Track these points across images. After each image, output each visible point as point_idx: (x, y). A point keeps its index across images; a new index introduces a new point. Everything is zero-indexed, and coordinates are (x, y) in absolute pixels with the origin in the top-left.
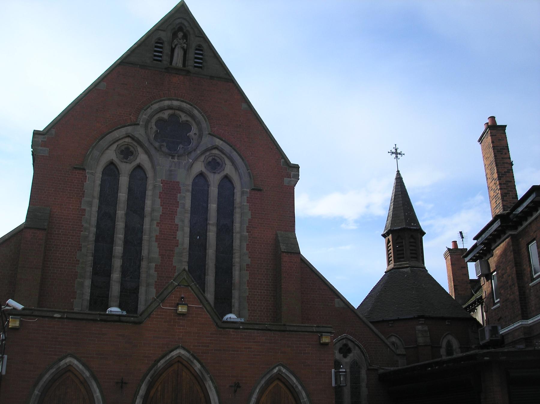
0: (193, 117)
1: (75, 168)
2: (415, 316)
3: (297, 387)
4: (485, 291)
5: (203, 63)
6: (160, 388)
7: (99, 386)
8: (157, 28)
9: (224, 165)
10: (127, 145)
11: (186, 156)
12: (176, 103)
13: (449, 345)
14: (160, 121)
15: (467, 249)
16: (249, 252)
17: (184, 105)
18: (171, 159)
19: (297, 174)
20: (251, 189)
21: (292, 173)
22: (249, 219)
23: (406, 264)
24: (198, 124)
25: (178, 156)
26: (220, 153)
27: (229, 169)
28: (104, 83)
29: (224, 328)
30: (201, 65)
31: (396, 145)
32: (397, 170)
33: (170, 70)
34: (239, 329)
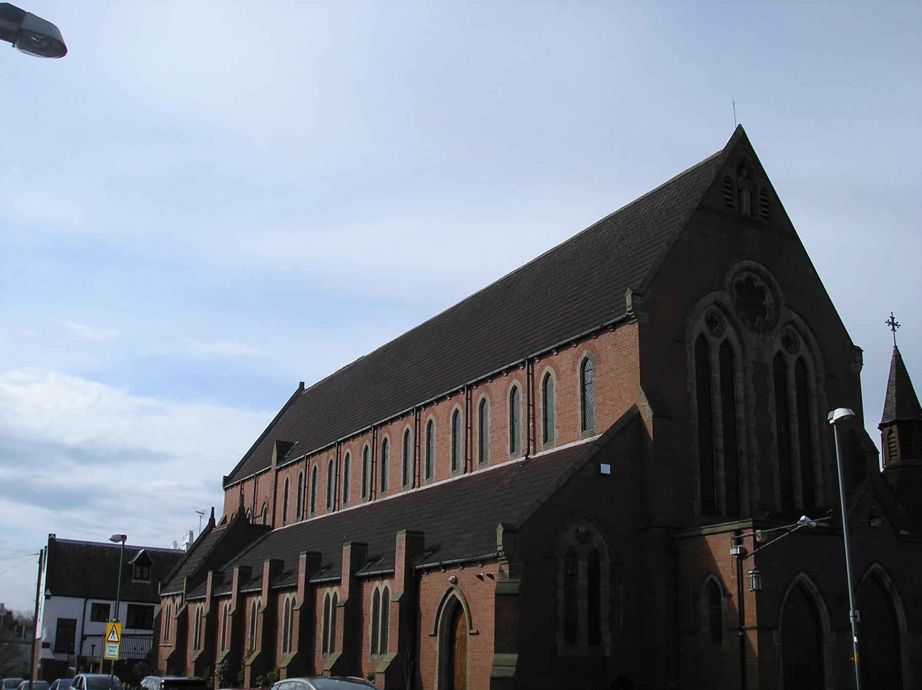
14: (739, 284)
15: (633, 417)
27: (803, 349)
31: (892, 313)
32: (894, 345)
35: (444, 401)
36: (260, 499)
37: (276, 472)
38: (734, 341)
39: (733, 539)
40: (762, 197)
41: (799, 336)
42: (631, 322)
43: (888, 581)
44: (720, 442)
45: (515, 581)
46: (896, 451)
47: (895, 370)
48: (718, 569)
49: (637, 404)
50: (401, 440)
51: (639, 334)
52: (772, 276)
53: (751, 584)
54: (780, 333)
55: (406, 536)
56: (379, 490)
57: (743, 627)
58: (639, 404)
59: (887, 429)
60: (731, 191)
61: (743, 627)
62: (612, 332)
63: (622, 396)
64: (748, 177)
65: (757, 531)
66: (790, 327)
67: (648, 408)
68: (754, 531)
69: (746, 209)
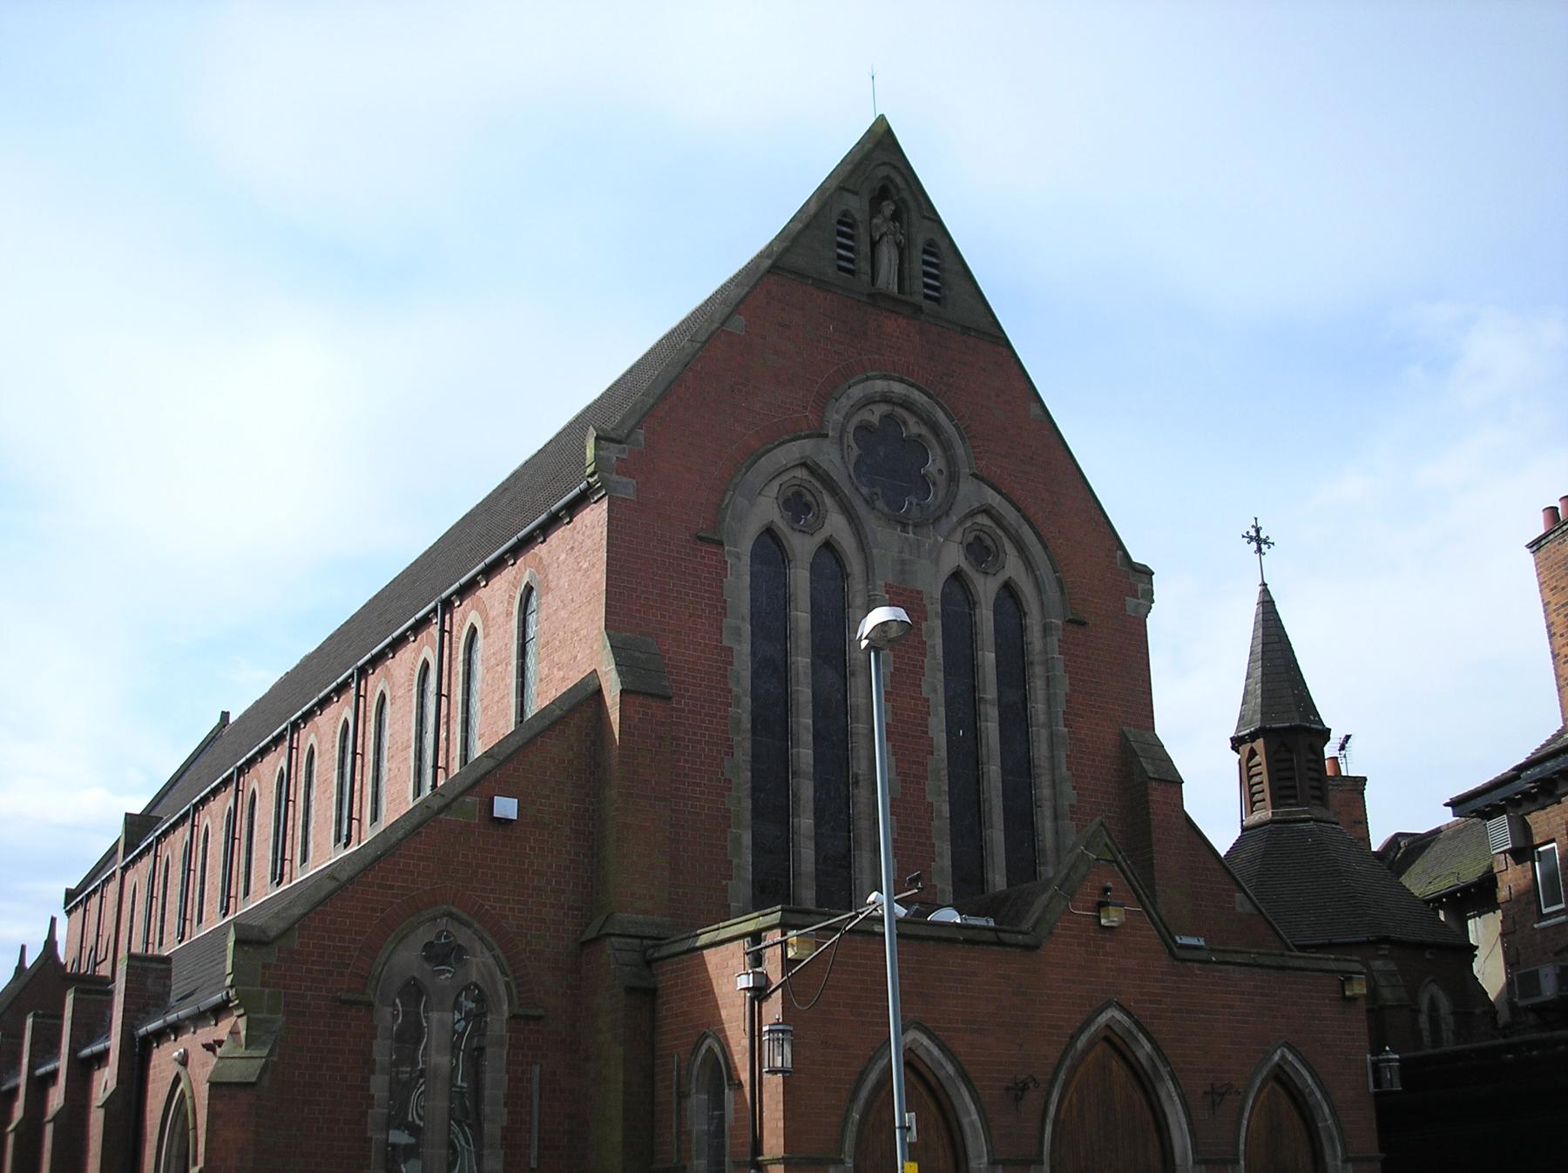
0: (935, 428)
1: (701, 539)
2: (1371, 938)
3: (1312, 1093)
4: (1509, 886)
5: (942, 291)
6: (1074, 1101)
7: (976, 1100)
8: (842, 185)
9: (1002, 555)
10: (799, 486)
11: (931, 527)
12: (898, 388)
13: (1433, 1001)
14: (864, 429)
15: (587, 696)
16: (1073, 775)
17: (916, 395)
18: (901, 531)
19: (1149, 589)
20: (1067, 619)
21: (1141, 586)
22: (1066, 694)
23: (1304, 812)
24: (946, 447)
25: (915, 526)
26: (994, 526)
27: (1013, 567)
28: (741, 317)
29: (1184, 960)
30: (936, 294)
31: (1256, 519)
32: (1260, 582)
33: (876, 298)
34: (1210, 962)
35: (330, 706)
36: (740, 1006)
37: (122, 873)
38: (847, 543)
39: (748, 954)
40: (927, 258)
41: (1005, 539)
42: (596, 498)
43: (1144, 1049)
44: (804, 755)
45: (256, 1053)
46: (1263, 791)
47: (1261, 630)
48: (723, 1024)
49: (598, 671)
50: (272, 792)
51: (608, 521)
52: (941, 416)
53: (778, 1056)
54: (960, 530)
55: (128, 965)
56: (241, 895)
57: (760, 1158)
58: (602, 670)
59: (1245, 748)
60: (939, 293)
61: (760, 1158)
62: (568, 523)
63: (576, 656)
64: (895, 217)
65: (791, 933)
66: (983, 520)
67: (614, 675)
68: (784, 934)
69: (887, 277)
